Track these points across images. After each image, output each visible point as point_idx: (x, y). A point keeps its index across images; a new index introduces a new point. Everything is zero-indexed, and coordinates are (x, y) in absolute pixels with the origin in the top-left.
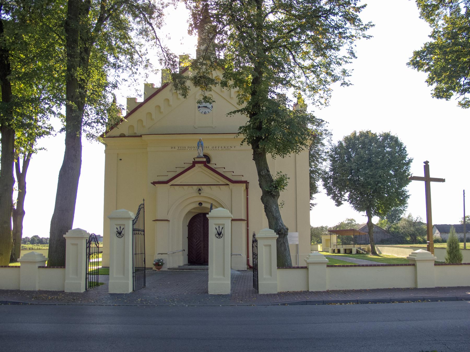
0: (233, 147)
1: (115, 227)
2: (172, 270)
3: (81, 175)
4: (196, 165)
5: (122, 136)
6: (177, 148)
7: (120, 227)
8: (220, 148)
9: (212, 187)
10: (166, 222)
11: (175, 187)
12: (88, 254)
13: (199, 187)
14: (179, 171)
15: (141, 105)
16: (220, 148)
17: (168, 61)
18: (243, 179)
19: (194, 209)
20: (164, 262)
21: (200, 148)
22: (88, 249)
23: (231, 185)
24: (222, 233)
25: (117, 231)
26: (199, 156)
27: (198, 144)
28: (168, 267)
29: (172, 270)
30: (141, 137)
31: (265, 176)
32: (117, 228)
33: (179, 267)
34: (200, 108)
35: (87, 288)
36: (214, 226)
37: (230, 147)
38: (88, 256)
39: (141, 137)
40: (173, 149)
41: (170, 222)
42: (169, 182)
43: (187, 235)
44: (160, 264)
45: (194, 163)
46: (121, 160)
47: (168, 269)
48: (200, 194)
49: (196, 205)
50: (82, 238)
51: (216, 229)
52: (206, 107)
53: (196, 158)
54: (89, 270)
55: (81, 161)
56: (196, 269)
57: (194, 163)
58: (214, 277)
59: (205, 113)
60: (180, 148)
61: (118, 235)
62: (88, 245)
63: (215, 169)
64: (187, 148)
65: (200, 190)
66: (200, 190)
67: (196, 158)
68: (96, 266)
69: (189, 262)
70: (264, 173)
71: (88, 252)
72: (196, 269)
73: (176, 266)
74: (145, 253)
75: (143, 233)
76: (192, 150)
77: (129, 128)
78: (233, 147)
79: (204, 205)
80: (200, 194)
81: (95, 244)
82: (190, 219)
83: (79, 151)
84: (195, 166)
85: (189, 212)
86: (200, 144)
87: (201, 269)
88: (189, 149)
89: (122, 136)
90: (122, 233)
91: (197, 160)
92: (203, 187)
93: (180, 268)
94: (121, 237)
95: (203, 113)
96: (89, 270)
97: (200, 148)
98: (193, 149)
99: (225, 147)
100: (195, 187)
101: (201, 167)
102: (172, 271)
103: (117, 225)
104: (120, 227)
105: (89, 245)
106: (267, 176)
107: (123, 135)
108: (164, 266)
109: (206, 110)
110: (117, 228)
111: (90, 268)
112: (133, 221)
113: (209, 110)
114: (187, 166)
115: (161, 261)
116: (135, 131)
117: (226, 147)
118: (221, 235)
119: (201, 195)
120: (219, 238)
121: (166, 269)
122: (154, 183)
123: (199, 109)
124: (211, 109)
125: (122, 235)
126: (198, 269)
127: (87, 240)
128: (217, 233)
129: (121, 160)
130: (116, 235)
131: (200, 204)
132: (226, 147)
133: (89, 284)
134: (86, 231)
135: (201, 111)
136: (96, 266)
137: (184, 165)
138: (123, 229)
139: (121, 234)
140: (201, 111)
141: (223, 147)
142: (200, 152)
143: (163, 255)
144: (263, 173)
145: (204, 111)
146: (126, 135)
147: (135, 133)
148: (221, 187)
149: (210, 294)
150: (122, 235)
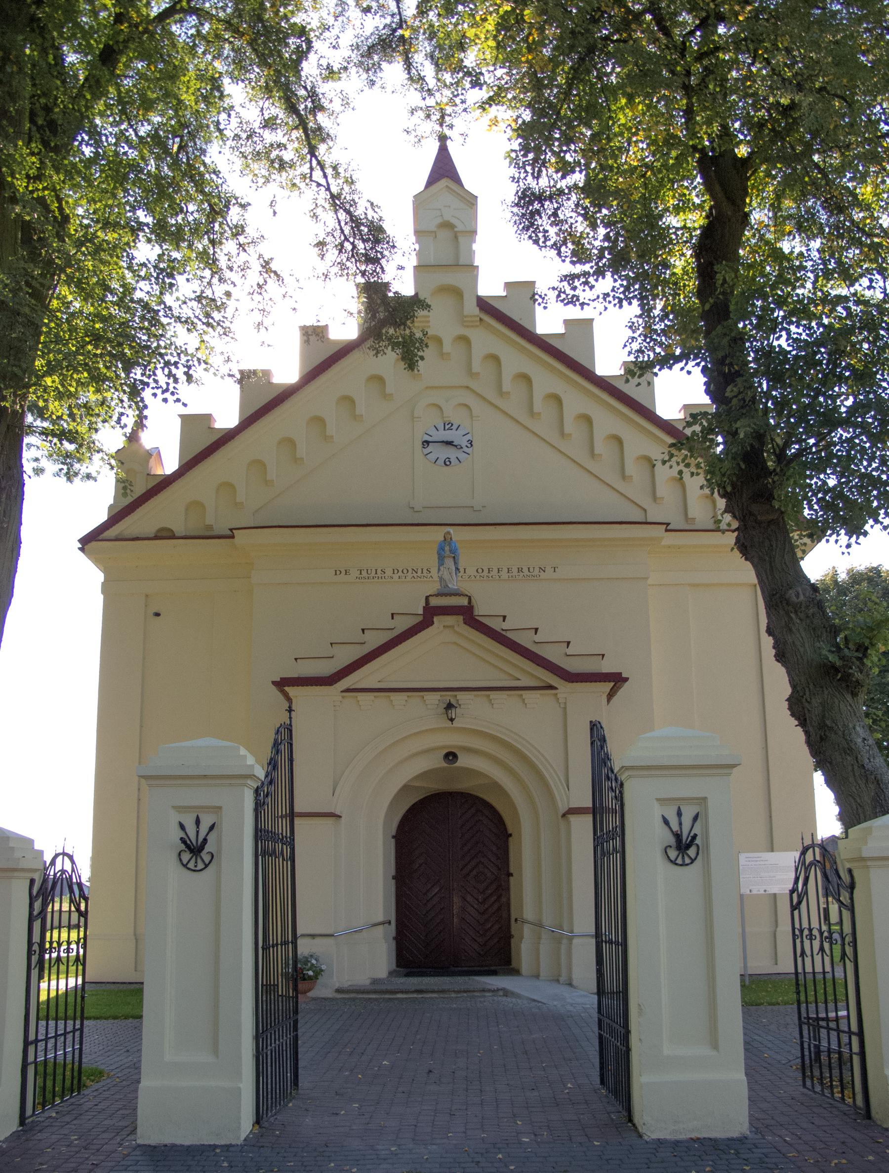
0: (549, 570)
1: (174, 818)
2: (352, 995)
3: (14, 600)
4: (436, 619)
5: (165, 535)
6: (355, 573)
7: (198, 822)
8: (504, 574)
9: (493, 695)
10: (330, 821)
11: (361, 696)
12: (36, 947)
13: (448, 697)
14: (375, 640)
15: (229, 436)
16: (504, 574)
17: (351, 240)
18: (606, 667)
19: (423, 775)
20: (324, 967)
21: (449, 563)
22: (37, 925)
23: (565, 689)
24: (698, 841)
25: (183, 840)
26: (446, 591)
27: (441, 548)
28: (337, 986)
29: (352, 995)
30: (233, 537)
31: (807, 607)
32: (182, 827)
33: (375, 981)
34: (431, 448)
35: (29, 1112)
36: (658, 811)
37: (537, 569)
38: (35, 959)
39: (233, 537)
40: (342, 578)
41: (343, 819)
42: (339, 680)
43: (392, 871)
44: (311, 973)
45: (430, 614)
46: (157, 615)
47: (338, 991)
48: (452, 720)
49: (436, 762)
50: (10, 872)
51: (666, 822)
52: (449, 443)
53: (437, 595)
54: (43, 997)
55: (18, 542)
56: (443, 991)
57: (430, 614)
58: (666, 1051)
59: (447, 463)
60: (364, 573)
61: (186, 857)
62: (37, 905)
63: (504, 633)
64: (389, 572)
65: (450, 706)
66: (450, 706)
67: (437, 595)
68: (62, 976)
69: (398, 965)
70: (802, 597)
71: (36, 938)
72: (443, 991)
73: (362, 979)
74: (861, 1034)
75: (287, 850)
76: (408, 579)
77: (187, 509)
78: (549, 570)
79: (463, 761)
80: (452, 720)
81: (71, 901)
82: (407, 808)
83: (8, 497)
84: (433, 623)
85: (406, 789)
86: (447, 548)
87: (459, 992)
88: (396, 576)
89: (165, 535)
90: (208, 848)
91: (435, 602)
92: (461, 696)
93: (376, 988)
94: (200, 866)
95: (441, 462)
96: (43, 997)
97: (449, 563)
98: (410, 575)
99: (520, 570)
100: (433, 698)
101: (453, 627)
102: (354, 999)
103: (179, 809)
104: (198, 822)
105: (44, 905)
106: (816, 610)
107: (164, 534)
108: (321, 980)
109: (452, 453)
110: (182, 827)
111: (44, 985)
112: (257, 791)
113: (462, 456)
114: (402, 624)
115: (314, 962)
116: (209, 520)
117: (525, 570)
118: (692, 852)
119: (456, 724)
120: (684, 865)
121: (328, 993)
122: (282, 684)
123: (426, 451)
124: (465, 449)
125: (207, 859)
126: (449, 991)
127: (32, 882)
128: (672, 841)
129: (157, 615)
130: (175, 855)
131: (451, 756)
132: (525, 570)
133: (40, 1081)
134: (31, 842)
135: (432, 457)
136: (62, 976)
137: (391, 624)
138: (212, 828)
139: (204, 854)
140: (432, 457)
141: (515, 570)
142: (446, 576)
143: (318, 941)
144: (798, 596)
145: (443, 457)
146: (177, 535)
147: (210, 527)
148: (526, 694)
149: (654, 1136)
150: (207, 859)
